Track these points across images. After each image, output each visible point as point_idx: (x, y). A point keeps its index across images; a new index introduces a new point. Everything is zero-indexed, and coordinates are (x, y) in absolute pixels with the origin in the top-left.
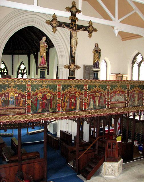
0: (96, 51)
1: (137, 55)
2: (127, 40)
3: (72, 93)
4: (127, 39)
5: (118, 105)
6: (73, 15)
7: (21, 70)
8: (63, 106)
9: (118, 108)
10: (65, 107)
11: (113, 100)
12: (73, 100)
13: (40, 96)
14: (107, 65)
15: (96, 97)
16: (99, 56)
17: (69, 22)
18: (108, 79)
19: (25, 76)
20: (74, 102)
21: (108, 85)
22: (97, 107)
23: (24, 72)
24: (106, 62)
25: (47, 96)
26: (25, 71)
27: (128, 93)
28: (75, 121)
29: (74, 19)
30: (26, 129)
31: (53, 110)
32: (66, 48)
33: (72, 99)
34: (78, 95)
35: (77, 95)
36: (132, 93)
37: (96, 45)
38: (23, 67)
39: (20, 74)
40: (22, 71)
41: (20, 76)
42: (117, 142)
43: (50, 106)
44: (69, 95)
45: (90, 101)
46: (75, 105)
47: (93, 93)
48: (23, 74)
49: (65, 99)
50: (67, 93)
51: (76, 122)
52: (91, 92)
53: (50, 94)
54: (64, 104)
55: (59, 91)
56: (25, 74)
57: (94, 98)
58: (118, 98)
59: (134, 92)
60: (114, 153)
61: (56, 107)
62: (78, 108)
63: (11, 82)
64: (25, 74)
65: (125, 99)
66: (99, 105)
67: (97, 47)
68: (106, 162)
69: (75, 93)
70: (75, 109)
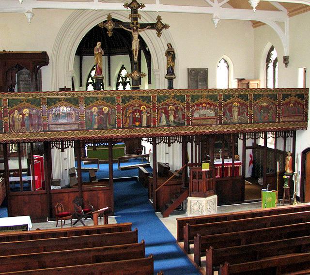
0: (168, 52)
1: (272, 49)
2: (296, 14)
4: (299, 11)
5: (205, 122)
6: (134, 11)
7: (122, 78)
8: (124, 122)
9: (205, 125)
11: (196, 115)
12: (137, 115)
13: (95, 110)
14: (228, 66)
15: (169, 111)
16: (174, 58)
18: (276, 87)
19: (128, 87)
20: (139, 117)
21: (188, 96)
22: (172, 124)
23: (127, 81)
24: (226, 62)
26: (128, 80)
27: (220, 105)
28: (149, 143)
29: (135, 17)
30: (117, 164)
31: (112, 127)
32: (161, 45)
33: (136, 114)
36: (228, 106)
37: (170, 46)
38: (124, 73)
39: (121, 84)
40: (124, 79)
41: (121, 87)
42: (203, 170)
45: (161, 116)
46: (140, 120)
47: (165, 106)
48: (124, 84)
51: (151, 143)
52: (162, 105)
55: (5, 107)
56: (128, 84)
57: (167, 113)
58: (203, 112)
59: (230, 105)
60: (200, 186)
61: (115, 122)
62: (144, 124)
64: (128, 84)
65: (216, 114)
66: (174, 122)
67: (170, 48)
68: (191, 196)
69: (140, 105)
70: (140, 126)
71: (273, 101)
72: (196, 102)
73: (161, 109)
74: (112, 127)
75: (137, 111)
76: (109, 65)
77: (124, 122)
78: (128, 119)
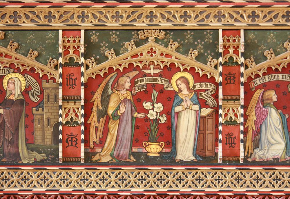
3: (145, 75)
10: (110, 141)
12: (154, 110)
25: (5, 84)
33: (147, 105)
34: (187, 82)
35: (176, 84)
43: (22, 132)
44: (132, 81)
46: (167, 134)
49: (105, 100)
50: (120, 74)
53: (20, 76)
54: (101, 126)
55: (70, 63)
62: (185, 150)
63: (236, 20)
69: (170, 70)
70: (168, 159)
71: (197, 65)
72: (272, 60)
73: (265, 87)
74: (40, 157)
75: (155, 94)
76: (188, 126)
77: (94, 138)
78: (113, 127)
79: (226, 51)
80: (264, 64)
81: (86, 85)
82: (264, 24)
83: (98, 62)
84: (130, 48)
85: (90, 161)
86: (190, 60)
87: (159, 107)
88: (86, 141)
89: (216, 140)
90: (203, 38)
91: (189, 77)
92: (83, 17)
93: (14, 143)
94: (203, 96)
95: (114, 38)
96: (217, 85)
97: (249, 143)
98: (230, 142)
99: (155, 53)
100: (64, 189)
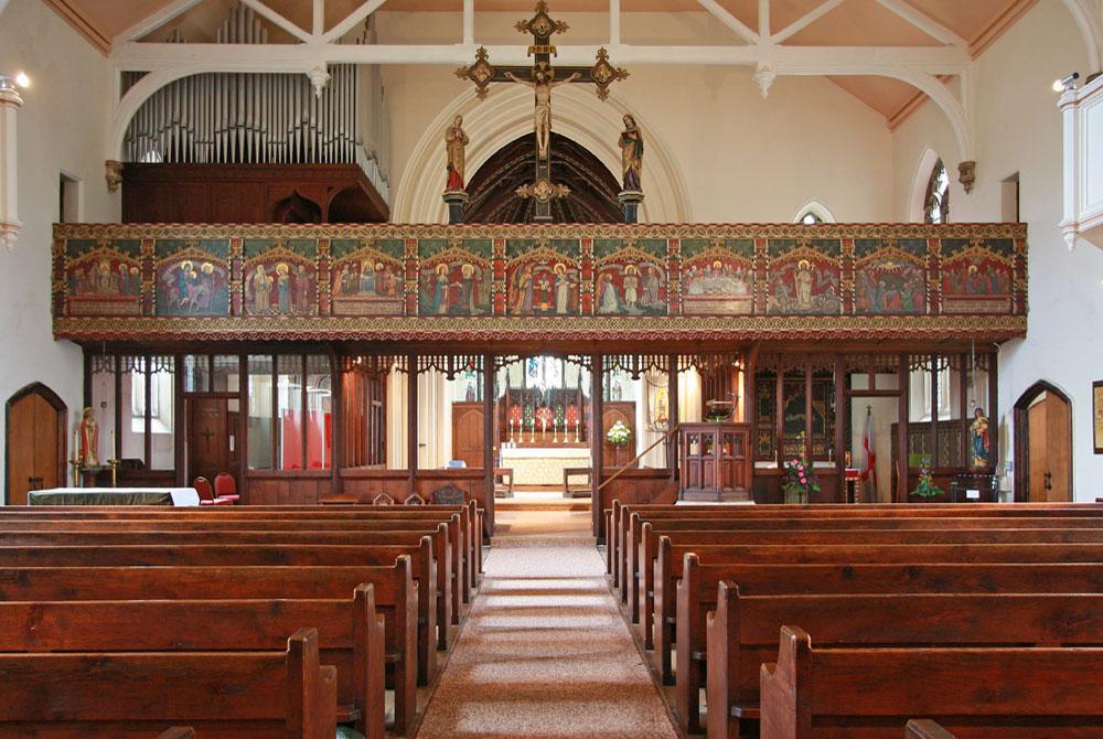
0: (625, 135)
6: (542, 40)
10: (520, 303)
12: (544, 285)
17: (531, 61)
29: (542, 52)
33: (541, 282)
43: (472, 297)
44: (532, 269)
46: (552, 297)
49: (517, 279)
50: (526, 264)
62: (562, 309)
69: (552, 263)
70: (552, 313)
71: (568, 259)
72: (609, 257)
73: (605, 271)
74: (482, 311)
75: (545, 275)
77: (511, 300)
79: (584, 252)
80: (605, 259)
81: (507, 271)
82: (604, 237)
83: (688, 257)
84: (531, 250)
85: (509, 314)
86: (564, 256)
87: (547, 283)
88: (507, 303)
89: (579, 302)
90: (832, 244)
91: (563, 266)
92: (505, 232)
93: (468, 303)
94: (572, 276)
95: (522, 244)
96: (579, 270)
97: (597, 304)
98: (586, 302)
99: (545, 253)
100: (495, 330)
